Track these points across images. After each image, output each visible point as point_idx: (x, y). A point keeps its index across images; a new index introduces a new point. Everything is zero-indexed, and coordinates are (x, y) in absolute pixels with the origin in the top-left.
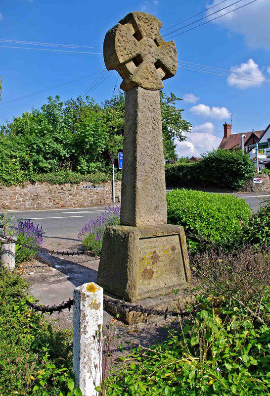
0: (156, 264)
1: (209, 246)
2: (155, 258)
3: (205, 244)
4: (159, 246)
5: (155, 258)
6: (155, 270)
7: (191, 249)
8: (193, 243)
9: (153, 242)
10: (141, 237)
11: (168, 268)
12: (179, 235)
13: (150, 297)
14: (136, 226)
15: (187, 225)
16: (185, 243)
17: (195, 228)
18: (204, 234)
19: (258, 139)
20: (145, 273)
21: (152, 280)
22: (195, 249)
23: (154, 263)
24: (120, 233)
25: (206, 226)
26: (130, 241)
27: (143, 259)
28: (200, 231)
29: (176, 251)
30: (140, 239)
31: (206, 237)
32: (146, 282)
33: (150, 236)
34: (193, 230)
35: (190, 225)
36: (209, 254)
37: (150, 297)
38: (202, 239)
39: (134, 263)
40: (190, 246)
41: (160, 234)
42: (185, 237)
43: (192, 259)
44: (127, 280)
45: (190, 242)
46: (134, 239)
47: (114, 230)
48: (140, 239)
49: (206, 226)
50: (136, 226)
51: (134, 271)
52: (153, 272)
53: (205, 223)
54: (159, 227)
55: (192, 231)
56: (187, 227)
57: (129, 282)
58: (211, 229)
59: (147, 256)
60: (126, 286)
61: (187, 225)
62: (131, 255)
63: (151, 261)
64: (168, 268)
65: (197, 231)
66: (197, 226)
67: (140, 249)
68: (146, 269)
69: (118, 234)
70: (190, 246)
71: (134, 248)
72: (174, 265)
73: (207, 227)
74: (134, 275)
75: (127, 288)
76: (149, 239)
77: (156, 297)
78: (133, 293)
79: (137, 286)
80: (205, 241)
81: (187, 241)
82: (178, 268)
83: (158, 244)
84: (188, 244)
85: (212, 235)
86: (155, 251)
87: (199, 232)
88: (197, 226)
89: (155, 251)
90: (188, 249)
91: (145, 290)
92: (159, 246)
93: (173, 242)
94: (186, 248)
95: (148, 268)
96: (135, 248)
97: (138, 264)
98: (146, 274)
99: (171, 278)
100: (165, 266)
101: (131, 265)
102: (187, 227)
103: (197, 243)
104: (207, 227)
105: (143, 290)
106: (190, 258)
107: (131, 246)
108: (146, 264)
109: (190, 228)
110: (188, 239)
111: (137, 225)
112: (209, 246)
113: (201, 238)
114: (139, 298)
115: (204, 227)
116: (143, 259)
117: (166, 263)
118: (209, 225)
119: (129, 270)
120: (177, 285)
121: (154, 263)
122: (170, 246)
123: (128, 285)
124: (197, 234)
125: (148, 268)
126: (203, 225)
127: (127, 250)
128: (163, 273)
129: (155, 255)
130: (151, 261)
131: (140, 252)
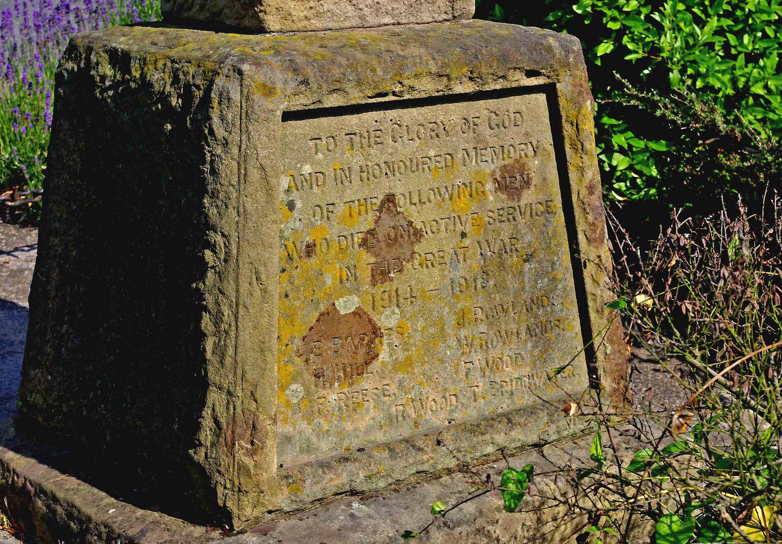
0: (397, 282)
1: (735, 161)
2: (393, 241)
3: (712, 150)
4: (414, 165)
5: (393, 241)
6: (387, 320)
7: (623, 178)
8: (640, 144)
9: (375, 138)
10: (301, 102)
11: (474, 304)
12: (550, 91)
13: (353, 493)
14: (260, 29)
15: (607, 34)
16: (591, 145)
17: (656, 50)
18: (708, 88)
19: (232, 528)
20: (324, 336)
21: (367, 383)
22: (650, 182)
23: (380, 274)
24: (159, 79)
25: (718, 41)
26: (220, 132)
27: (310, 249)
28: (683, 72)
29: (529, 197)
30: (288, 116)
31: (719, 110)
32: (333, 396)
33: (356, 97)
34: (642, 63)
35: (621, 32)
36: (755, 226)
37: (353, 493)
38: (696, 118)
39: (245, 270)
40: (620, 161)
41: (427, 87)
42: (590, 106)
43: (632, 257)
44: (203, 385)
45: (619, 140)
46: (246, 115)
47: (121, 60)
48: (288, 116)
49: (718, 41)
50: (260, 29)
51: (246, 324)
52: (376, 332)
53: (714, 23)
54: (420, 38)
55: (632, 71)
56: (605, 48)
57: (214, 397)
58: (752, 58)
59: (333, 231)
60: (198, 427)
61: (607, 34)
62: (228, 222)
63: (367, 259)
64: (474, 304)
65: (662, 70)
66: (665, 41)
67: (285, 182)
68: (329, 316)
69: (145, 84)
70: (620, 161)
71: (243, 177)
72: (511, 283)
73: (727, 46)
74: (248, 354)
75: (206, 435)
76: (352, 120)
77: (397, 487)
78: (242, 469)
79: (265, 423)
80: (711, 129)
81: (603, 136)
82: (540, 301)
83: (407, 149)
84: (609, 151)
85: (756, 97)
86: (390, 199)
87: (674, 76)
88: (665, 41)
89: (390, 199)
90: (608, 177)
91: (325, 448)
92: (414, 165)
93: (512, 136)
94: (593, 174)
95: (346, 305)
96: (255, 174)
97: (276, 287)
98: (329, 345)
99: (492, 366)
100: (456, 289)
101: (230, 290)
102: (605, 48)
103: (661, 146)
104: (727, 46)
105: (308, 449)
106: (616, 256)
107: (228, 167)
108: (329, 280)
109: (621, 50)
110: (606, 120)
111: (272, 21)
112: (735, 161)
113: (687, 111)
114: (282, 500)
115: (710, 46)
116: (310, 249)
117: (462, 271)
118: (739, 35)
119: (217, 320)
120: (531, 411)
121: (380, 274)
122: (491, 166)
123: (207, 422)
124: (666, 89)
125: (346, 305)
126: (704, 35)
127: (201, 190)
128: (443, 335)
129: (387, 221)
130: (367, 259)
131: (291, 206)
